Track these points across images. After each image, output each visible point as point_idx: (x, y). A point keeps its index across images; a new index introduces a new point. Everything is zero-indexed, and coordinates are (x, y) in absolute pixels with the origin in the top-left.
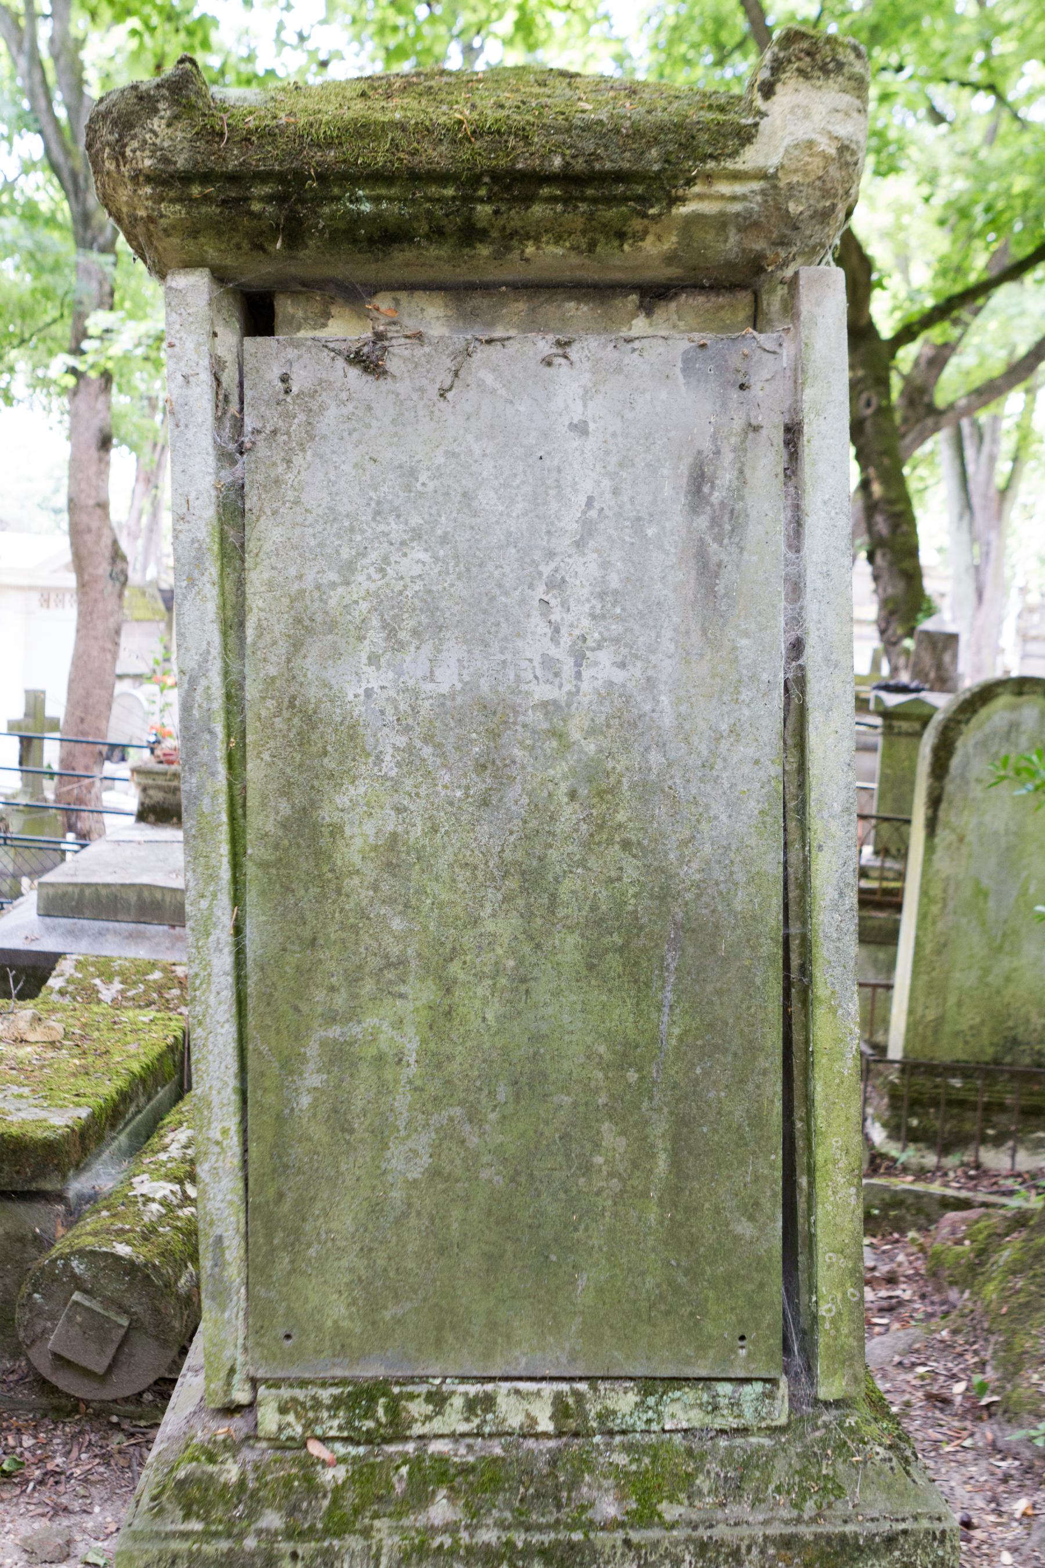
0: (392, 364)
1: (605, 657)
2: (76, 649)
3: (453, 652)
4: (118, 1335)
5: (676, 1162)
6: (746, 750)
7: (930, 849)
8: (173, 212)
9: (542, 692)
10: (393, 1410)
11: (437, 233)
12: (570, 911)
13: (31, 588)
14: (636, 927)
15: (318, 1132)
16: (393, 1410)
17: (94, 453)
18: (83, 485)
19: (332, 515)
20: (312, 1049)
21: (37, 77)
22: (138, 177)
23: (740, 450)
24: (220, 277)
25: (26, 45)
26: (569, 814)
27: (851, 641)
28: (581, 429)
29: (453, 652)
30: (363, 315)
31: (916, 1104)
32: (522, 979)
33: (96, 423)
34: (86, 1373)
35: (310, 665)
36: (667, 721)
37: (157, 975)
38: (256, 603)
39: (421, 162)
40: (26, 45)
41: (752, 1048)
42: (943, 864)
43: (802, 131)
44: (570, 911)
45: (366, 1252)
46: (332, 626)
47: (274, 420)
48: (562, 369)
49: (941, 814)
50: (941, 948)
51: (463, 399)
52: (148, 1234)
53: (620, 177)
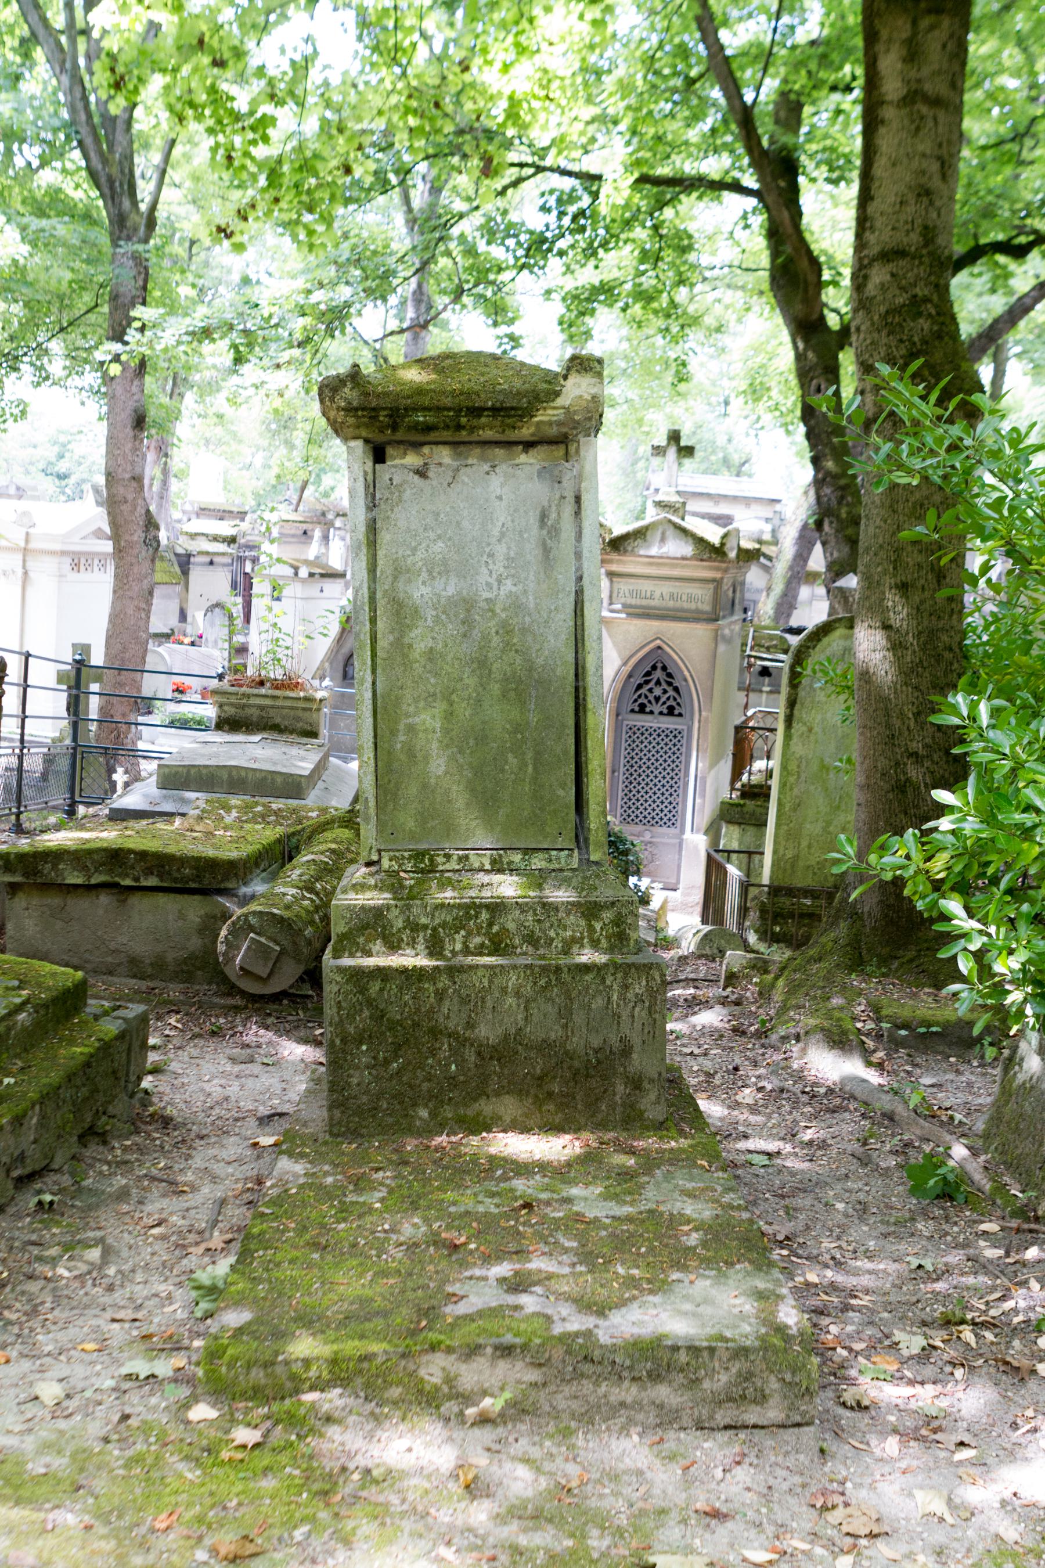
0: (430, 474)
1: (509, 582)
2: (113, 607)
3: (453, 580)
4: (274, 956)
5: (535, 768)
6: (561, 616)
7: (788, 737)
8: (351, 420)
9: (486, 595)
10: (431, 860)
11: (447, 427)
12: (496, 675)
13: (63, 553)
14: (520, 681)
15: (403, 757)
16: (431, 860)
17: (129, 431)
18: (120, 460)
19: (408, 530)
20: (401, 727)
21: (78, 94)
22: (338, 409)
23: (559, 505)
24: (367, 441)
25: (68, 65)
26: (496, 640)
27: (114, 524)
28: (500, 498)
29: (453, 580)
30: (419, 454)
31: (778, 916)
32: (479, 701)
33: (131, 405)
34: (258, 978)
35: (400, 585)
36: (532, 605)
37: (259, 808)
38: (380, 562)
39: (441, 404)
40: (68, 65)
41: (564, 726)
42: (798, 747)
43: (577, 392)
44: (496, 675)
45: (421, 802)
46: (408, 571)
47: (387, 495)
48: (493, 476)
49: (796, 712)
50: (797, 807)
51: (457, 487)
52: (288, 907)
53: (513, 408)
